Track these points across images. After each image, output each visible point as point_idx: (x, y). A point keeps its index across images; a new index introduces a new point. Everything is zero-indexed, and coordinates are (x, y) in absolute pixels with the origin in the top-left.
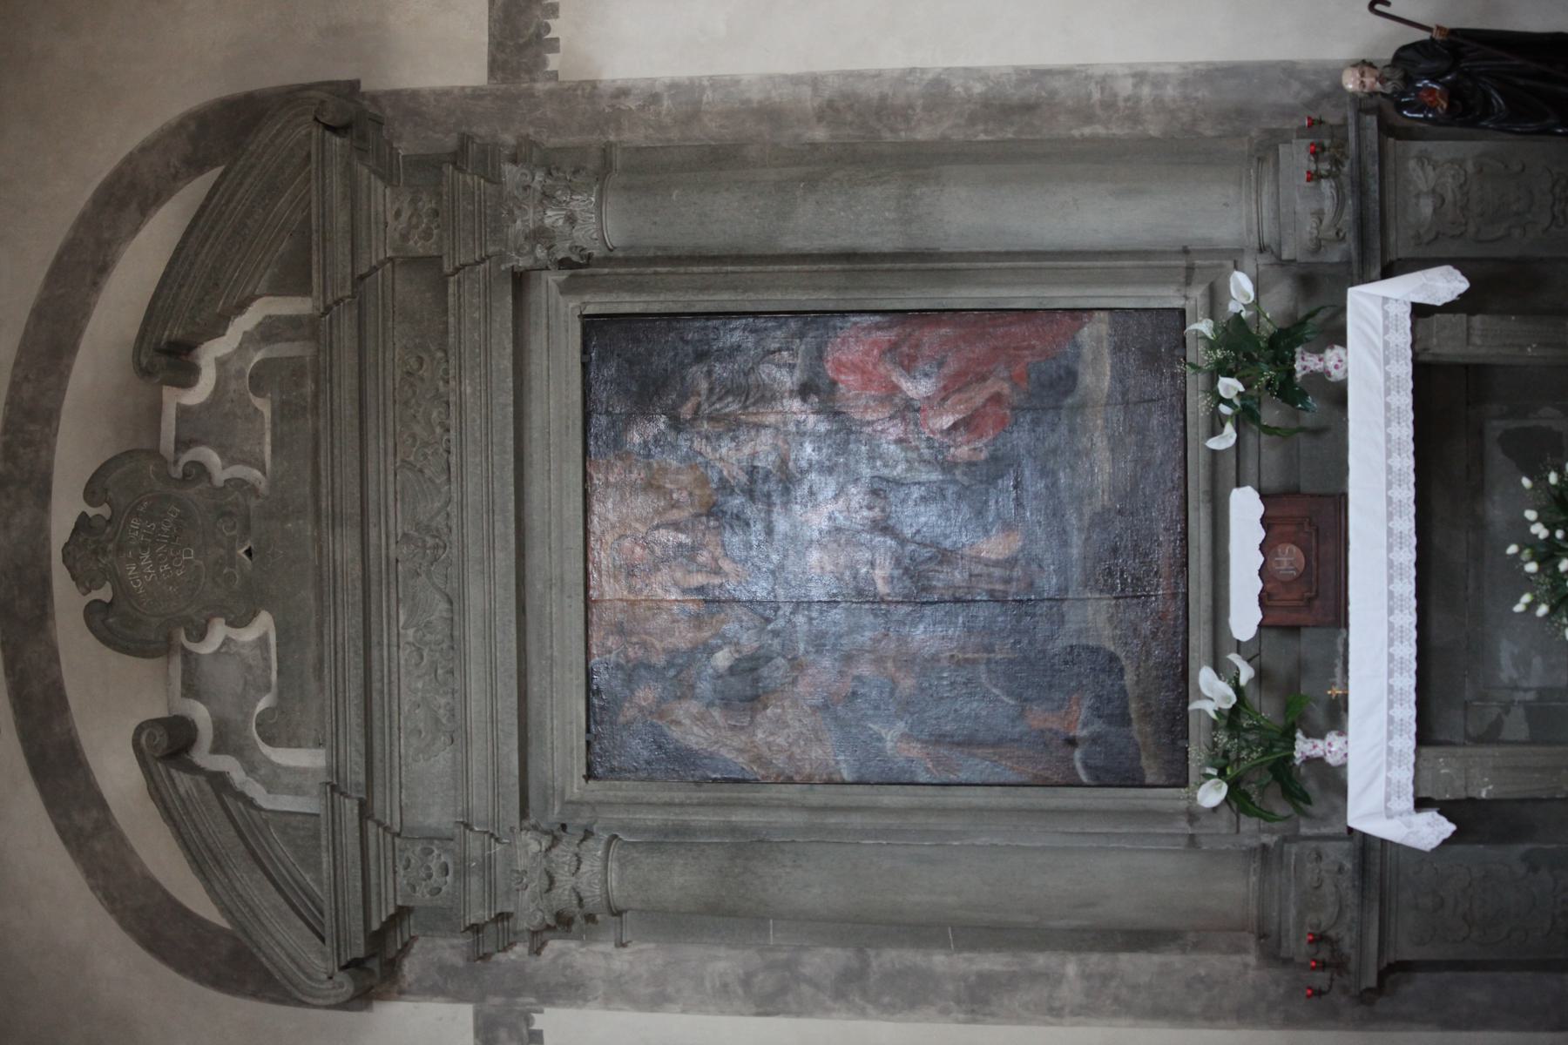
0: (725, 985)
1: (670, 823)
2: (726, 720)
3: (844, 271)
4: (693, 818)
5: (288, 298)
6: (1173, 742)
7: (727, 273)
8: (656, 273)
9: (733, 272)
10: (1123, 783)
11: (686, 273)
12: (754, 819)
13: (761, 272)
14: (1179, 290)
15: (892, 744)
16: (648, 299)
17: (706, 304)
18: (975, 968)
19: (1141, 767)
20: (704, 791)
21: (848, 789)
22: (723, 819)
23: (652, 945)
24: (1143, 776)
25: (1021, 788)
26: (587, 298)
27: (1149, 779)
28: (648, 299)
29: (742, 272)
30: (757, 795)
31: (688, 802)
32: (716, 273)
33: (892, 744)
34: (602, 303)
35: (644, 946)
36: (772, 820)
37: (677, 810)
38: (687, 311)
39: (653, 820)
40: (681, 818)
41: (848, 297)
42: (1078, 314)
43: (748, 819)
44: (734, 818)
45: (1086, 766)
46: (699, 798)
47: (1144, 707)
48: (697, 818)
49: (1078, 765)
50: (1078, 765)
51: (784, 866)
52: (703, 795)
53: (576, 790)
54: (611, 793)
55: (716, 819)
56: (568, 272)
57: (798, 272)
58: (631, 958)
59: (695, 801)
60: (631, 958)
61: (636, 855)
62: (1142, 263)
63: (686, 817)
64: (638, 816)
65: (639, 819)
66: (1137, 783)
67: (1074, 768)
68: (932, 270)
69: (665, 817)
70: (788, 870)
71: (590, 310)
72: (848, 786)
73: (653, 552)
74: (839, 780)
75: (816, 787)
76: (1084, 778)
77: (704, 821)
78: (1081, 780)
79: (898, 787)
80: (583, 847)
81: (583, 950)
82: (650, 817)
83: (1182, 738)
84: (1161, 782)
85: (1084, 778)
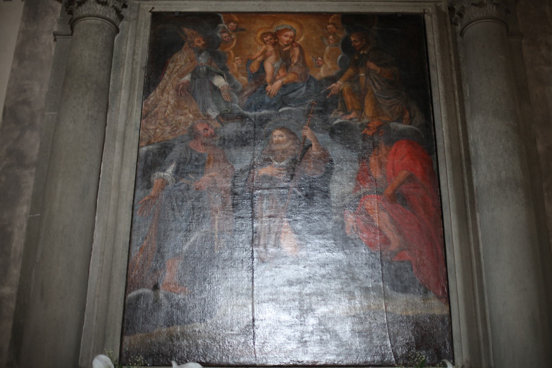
0: (25, 91)
1: (123, 58)
2: (183, 83)
3: (461, 155)
4: (125, 70)
5: (375, 12)
6: (151, 355)
7: (454, 92)
8: (450, 55)
9: (454, 96)
10: (125, 321)
11: (451, 70)
12: (121, 102)
13: (456, 110)
14: (467, 362)
15: (162, 176)
16: (436, 47)
17: (436, 76)
18: (16, 230)
19: (135, 333)
20: (140, 72)
21: (135, 150)
22: (123, 85)
23: (53, 54)
24: (129, 335)
25: (127, 254)
26: (434, 16)
27: (126, 339)
28: (436, 47)
29: (455, 100)
30: (136, 99)
31: (134, 63)
32: (453, 86)
33: (162, 176)
34: (432, 24)
35: (53, 49)
36: (120, 112)
37: (131, 61)
38: (431, 66)
39: (126, 49)
40: (126, 64)
41: (446, 154)
42: (447, 298)
43: (122, 99)
44: (123, 91)
45: (138, 297)
46: (136, 68)
47: (177, 335)
48: (125, 72)
49: (140, 291)
50: (140, 291)
51: (89, 110)
52: (138, 70)
53: (146, 6)
54: (143, 24)
55: (124, 82)
56: (447, 11)
57: (458, 130)
58: (47, 43)
59: (134, 67)
60: (47, 43)
61: (104, 34)
62: (481, 339)
63: (126, 67)
64: (129, 42)
65: (127, 43)
66: (125, 330)
67: (138, 288)
68: (466, 207)
69: (127, 56)
70: (86, 112)
71: (427, 18)
72: (137, 150)
73: (287, 46)
74: (141, 145)
75: (138, 131)
76: (132, 294)
77: (123, 75)
78: (130, 292)
79: (134, 179)
80: (112, 9)
81: (55, 20)
82: (128, 48)
83: (153, 361)
84: (124, 346)
85: (132, 294)
